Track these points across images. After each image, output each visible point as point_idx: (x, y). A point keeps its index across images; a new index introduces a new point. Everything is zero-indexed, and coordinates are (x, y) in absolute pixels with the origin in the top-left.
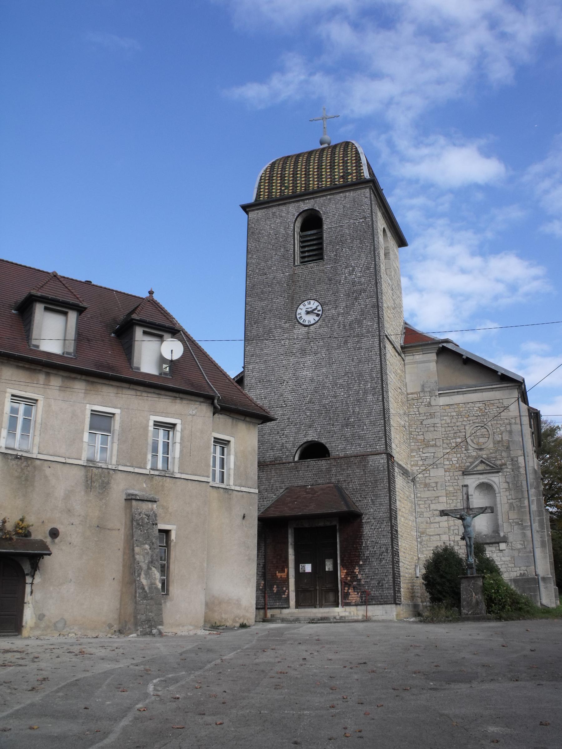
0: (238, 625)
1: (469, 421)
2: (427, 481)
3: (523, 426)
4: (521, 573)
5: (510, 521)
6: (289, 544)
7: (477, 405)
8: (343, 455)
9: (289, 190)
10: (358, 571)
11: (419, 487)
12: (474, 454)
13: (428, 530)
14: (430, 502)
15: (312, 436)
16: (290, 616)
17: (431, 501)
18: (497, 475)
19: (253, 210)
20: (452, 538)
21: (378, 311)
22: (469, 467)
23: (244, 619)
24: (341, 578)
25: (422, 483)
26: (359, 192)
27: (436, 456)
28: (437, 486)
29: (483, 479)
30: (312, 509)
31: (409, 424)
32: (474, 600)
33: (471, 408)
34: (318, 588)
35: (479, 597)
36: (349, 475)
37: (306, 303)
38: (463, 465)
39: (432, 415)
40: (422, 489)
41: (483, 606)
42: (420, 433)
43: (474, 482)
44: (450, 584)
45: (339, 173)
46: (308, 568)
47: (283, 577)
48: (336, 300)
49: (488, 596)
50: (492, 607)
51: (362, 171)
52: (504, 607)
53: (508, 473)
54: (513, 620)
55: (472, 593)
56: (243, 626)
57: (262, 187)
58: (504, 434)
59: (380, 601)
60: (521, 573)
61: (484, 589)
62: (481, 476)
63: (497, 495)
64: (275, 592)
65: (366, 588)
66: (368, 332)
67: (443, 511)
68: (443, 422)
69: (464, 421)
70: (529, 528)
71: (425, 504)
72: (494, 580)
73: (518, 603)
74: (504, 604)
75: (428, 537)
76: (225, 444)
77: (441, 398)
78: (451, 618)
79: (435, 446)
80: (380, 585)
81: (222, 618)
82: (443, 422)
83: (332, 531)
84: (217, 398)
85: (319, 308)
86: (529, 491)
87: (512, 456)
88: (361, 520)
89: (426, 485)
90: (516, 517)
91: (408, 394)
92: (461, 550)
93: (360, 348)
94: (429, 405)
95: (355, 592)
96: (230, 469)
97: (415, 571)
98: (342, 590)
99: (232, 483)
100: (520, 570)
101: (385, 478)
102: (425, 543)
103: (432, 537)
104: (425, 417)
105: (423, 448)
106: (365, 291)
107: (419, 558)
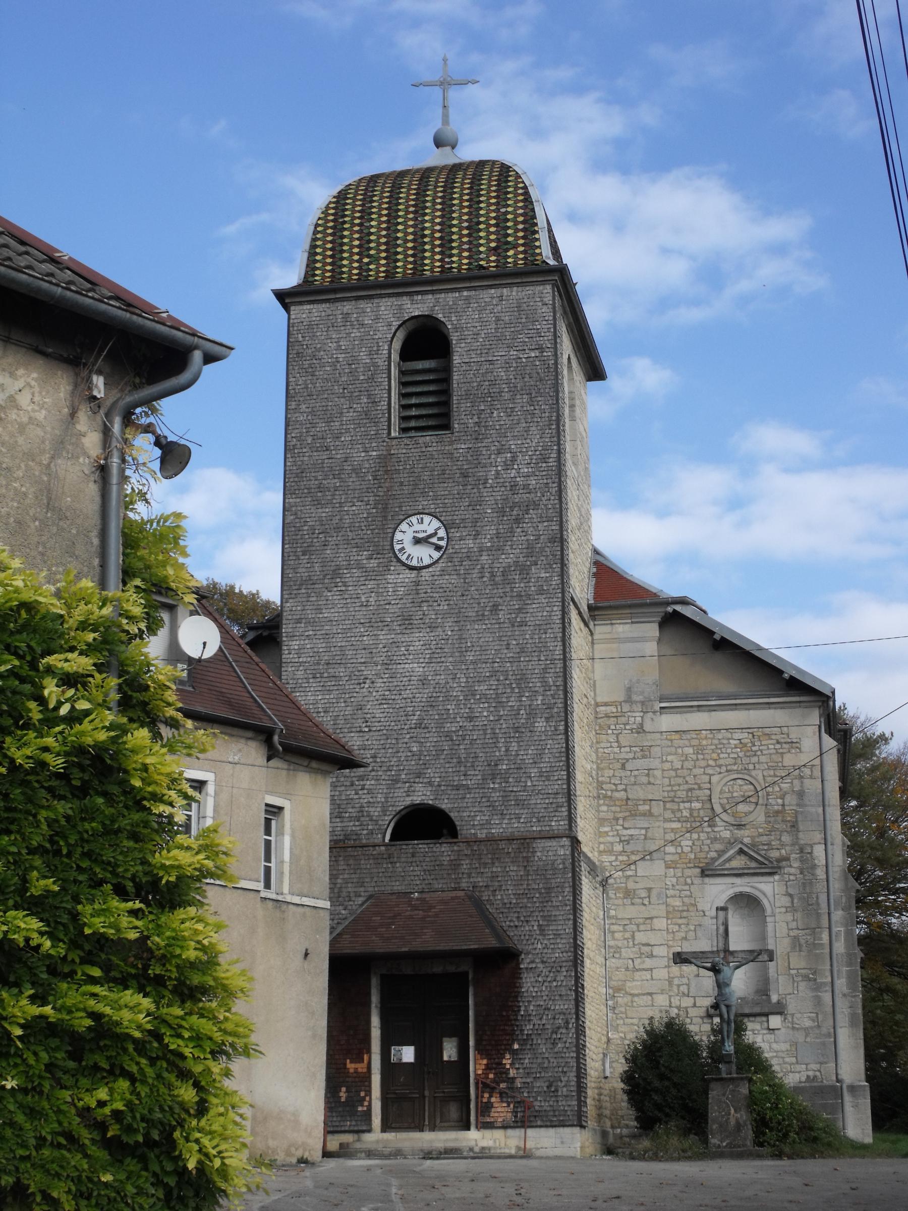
0: (294, 1160)
1: (720, 766)
2: (631, 885)
3: (825, 782)
4: (808, 1077)
5: (792, 972)
6: (373, 1005)
7: (736, 736)
8: (484, 836)
9: (379, 265)
10: (509, 1061)
11: (613, 896)
12: (727, 834)
13: (628, 984)
14: (635, 928)
15: (421, 795)
16: (381, 1145)
17: (638, 925)
18: (770, 879)
19: (301, 303)
20: (676, 1001)
21: (562, 550)
22: (714, 860)
23: (305, 1150)
24: (476, 1075)
25: (619, 888)
26: (529, 290)
27: (649, 835)
28: (649, 897)
29: (742, 885)
30: (427, 941)
31: (598, 768)
32: (733, 1122)
33: (725, 742)
34: (427, 1093)
35: (742, 1116)
36: (494, 877)
37: (414, 519)
38: (703, 855)
39: (645, 751)
40: (620, 902)
41: (748, 1133)
42: (620, 787)
43: (723, 891)
44: (679, 1091)
45: (489, 241)
46: (408, 1054)
47: (360, 1070)
48: (476, 521)
49: (758, 1114)
50: (764, 1134)
51: (537, 244)
52: (786, 1135)
53: (792, 878)
54: (803, 1158)
55: (726, 1108)
56: (302, 1161)
57: (318, 250)
58: (788, 799)
59: (551, 1121)
60: (808, 1077)
61: (752, 1101)
62: (738, 881)
63: (768, 919)
64: (343, 1100)
65: (525, 1094)
66: (541, 591)
67: (679, 953)
68: (667, 766)
69: (708, 766)
70: (829, 988)
71: (625, 931)
72: (770, 1086)
73: (811, 1129)
74: (786, 1127)
75: (629, 998)
76: (274, 814)
77: (664, 716)
78: (690, 1154)
79: (650, 814)
80: (552, 1089)
81: (268, 1148)
82: (667, 766)
83: (459, 984)
84: (278, 731)
85: (442, 533)
86: (832, 915)
87: (802, 842)
88: (518, 964)
89: (629, 894)
90: (803, 964)
91: (597, 705)
92: (700, 1030)
93: (523, 624)
94: (640, 729)
95: (502, 1102)
96: (282, 862)
97: (604, 1065)
98: (477, 1097)
99: (286, 890)
100: (807, 1070)
101: (567, 885)
102: (623, 1009)
103: (636, 999)
104: (631, 755)
105: (624, 819)
106: (536, 506)
107: (609, 1040)
